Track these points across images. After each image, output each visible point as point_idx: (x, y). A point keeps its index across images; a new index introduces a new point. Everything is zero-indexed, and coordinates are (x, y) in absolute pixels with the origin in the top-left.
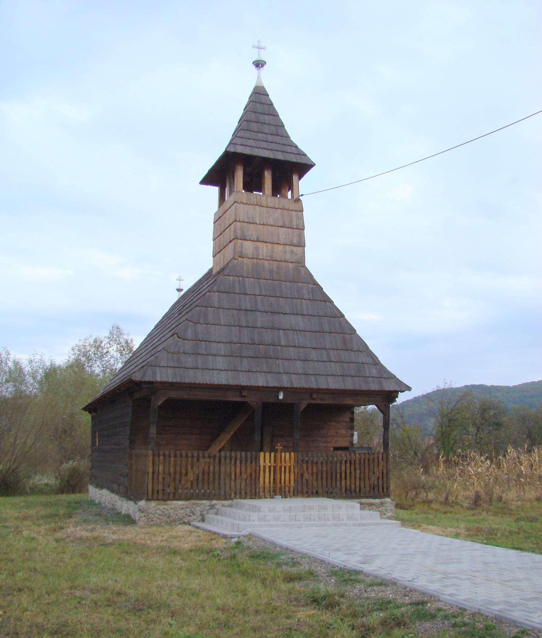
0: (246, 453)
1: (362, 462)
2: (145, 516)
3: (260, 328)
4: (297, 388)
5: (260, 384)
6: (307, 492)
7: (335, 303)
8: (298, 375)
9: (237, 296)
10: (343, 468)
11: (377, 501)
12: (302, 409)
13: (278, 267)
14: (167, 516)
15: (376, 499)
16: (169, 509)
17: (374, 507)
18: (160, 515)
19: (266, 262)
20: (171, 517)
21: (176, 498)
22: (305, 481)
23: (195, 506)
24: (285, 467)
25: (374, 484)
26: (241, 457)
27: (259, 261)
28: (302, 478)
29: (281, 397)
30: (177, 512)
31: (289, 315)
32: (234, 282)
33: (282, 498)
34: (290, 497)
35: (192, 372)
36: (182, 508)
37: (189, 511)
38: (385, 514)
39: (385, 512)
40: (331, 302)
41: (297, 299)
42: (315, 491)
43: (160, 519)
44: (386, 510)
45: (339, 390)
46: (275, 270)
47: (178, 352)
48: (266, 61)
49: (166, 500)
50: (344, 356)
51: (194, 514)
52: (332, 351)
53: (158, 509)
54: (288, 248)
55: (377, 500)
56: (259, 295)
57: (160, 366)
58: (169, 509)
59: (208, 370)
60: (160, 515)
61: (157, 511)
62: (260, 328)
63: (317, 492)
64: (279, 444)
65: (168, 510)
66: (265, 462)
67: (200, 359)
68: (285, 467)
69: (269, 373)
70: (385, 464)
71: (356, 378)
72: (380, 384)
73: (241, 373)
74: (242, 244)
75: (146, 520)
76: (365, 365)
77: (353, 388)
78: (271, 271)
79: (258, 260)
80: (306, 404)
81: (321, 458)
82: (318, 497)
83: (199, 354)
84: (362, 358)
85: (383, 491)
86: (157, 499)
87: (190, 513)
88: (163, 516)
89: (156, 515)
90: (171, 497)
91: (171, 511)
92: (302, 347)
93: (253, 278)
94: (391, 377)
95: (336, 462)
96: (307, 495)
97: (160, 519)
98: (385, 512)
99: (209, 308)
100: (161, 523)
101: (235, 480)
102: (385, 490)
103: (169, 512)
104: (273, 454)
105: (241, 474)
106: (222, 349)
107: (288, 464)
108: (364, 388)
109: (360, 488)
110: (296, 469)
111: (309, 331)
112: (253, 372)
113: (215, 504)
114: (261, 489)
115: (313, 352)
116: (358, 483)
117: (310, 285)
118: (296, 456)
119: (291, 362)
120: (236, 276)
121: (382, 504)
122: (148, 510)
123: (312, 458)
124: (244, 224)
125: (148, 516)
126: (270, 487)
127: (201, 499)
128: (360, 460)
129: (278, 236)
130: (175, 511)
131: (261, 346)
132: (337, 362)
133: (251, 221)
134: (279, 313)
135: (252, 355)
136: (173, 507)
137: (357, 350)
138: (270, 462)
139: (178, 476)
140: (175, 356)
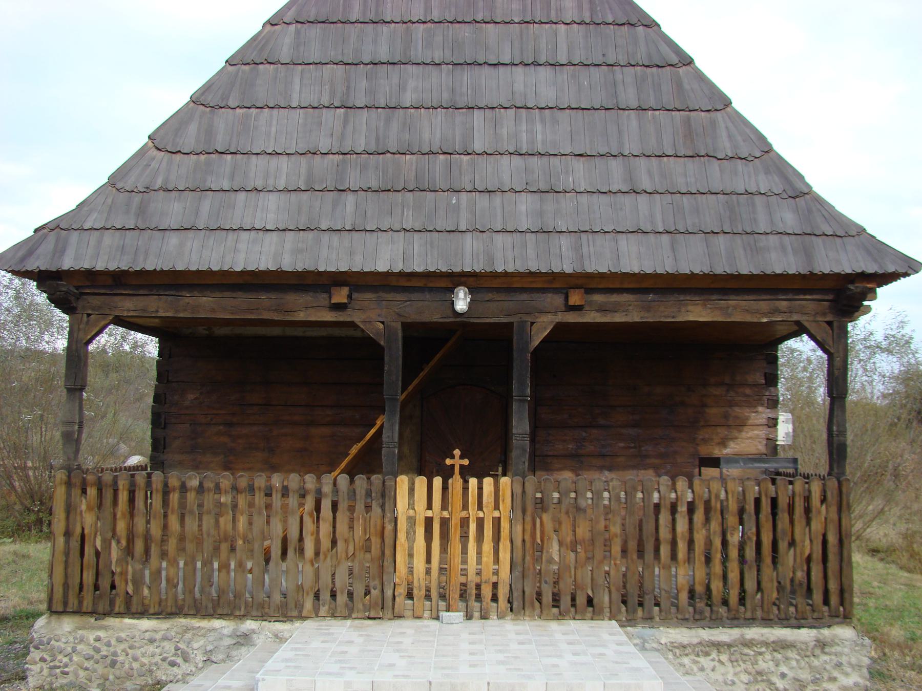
0: (369, 478)
2: (43, 660)
4: (506, 274)
9: (353, 30)
10: (682, 525)
11: (806, 635)
12: (536, 342)
14: (108, 660)
15: (799, 627)
17: (791, 654)
20: (118, 665)
23: (188, 636)
24: (480, 523)
25: (792, 580)
29: (462, 302)
30: (138, 653)
33: (469, 617)
34: (501, 617)
35: (173, 240)
36: (152, 641)
38: (833, 679)
39: (835, 674)
40: (651, 24)
43: (87, 669)
44: (839, 665)
45: (656, 276)
51: (186, 660)
53: (82, 641)
55: (804, 631)
58: (113, 642)
63: (590, 602)
64: (457, 452)
65: (108, 644)
66: (411, 505)
67: (207, 203)
68: (480, 523)
70: (834, 515)
71: (721, 237)
72: (808, 254)
73: (326, 237)
76: (758, 200)
77: (706, 270)
81: (606, 494)
83: (210, 190)
85: (826, 602)
86: (78, 612)
87: (175, 655)
89: (75, 658)
90: (119, 605)
95: (657, 507)
96: (555, 610)
98: (835, 674)
99: (261, 66)
102: (834, 599)
103: (112, 649)
104: (438, 481)
107: (489, 514)
108: (745, 267)
109: (743, 590)
110: (519, 528)
113: (253, 631)
114: (401, 591)
115: (579, 165)
116: (734, 576)
118: (518, 489)
119: (498, 199)
121: (822, 645)
122: (53, 642)
130: (131, 647)
131: (408, 157)
136: (123, 635)
138: (430, 506)
139: (139, 546)
140: (137, 198)
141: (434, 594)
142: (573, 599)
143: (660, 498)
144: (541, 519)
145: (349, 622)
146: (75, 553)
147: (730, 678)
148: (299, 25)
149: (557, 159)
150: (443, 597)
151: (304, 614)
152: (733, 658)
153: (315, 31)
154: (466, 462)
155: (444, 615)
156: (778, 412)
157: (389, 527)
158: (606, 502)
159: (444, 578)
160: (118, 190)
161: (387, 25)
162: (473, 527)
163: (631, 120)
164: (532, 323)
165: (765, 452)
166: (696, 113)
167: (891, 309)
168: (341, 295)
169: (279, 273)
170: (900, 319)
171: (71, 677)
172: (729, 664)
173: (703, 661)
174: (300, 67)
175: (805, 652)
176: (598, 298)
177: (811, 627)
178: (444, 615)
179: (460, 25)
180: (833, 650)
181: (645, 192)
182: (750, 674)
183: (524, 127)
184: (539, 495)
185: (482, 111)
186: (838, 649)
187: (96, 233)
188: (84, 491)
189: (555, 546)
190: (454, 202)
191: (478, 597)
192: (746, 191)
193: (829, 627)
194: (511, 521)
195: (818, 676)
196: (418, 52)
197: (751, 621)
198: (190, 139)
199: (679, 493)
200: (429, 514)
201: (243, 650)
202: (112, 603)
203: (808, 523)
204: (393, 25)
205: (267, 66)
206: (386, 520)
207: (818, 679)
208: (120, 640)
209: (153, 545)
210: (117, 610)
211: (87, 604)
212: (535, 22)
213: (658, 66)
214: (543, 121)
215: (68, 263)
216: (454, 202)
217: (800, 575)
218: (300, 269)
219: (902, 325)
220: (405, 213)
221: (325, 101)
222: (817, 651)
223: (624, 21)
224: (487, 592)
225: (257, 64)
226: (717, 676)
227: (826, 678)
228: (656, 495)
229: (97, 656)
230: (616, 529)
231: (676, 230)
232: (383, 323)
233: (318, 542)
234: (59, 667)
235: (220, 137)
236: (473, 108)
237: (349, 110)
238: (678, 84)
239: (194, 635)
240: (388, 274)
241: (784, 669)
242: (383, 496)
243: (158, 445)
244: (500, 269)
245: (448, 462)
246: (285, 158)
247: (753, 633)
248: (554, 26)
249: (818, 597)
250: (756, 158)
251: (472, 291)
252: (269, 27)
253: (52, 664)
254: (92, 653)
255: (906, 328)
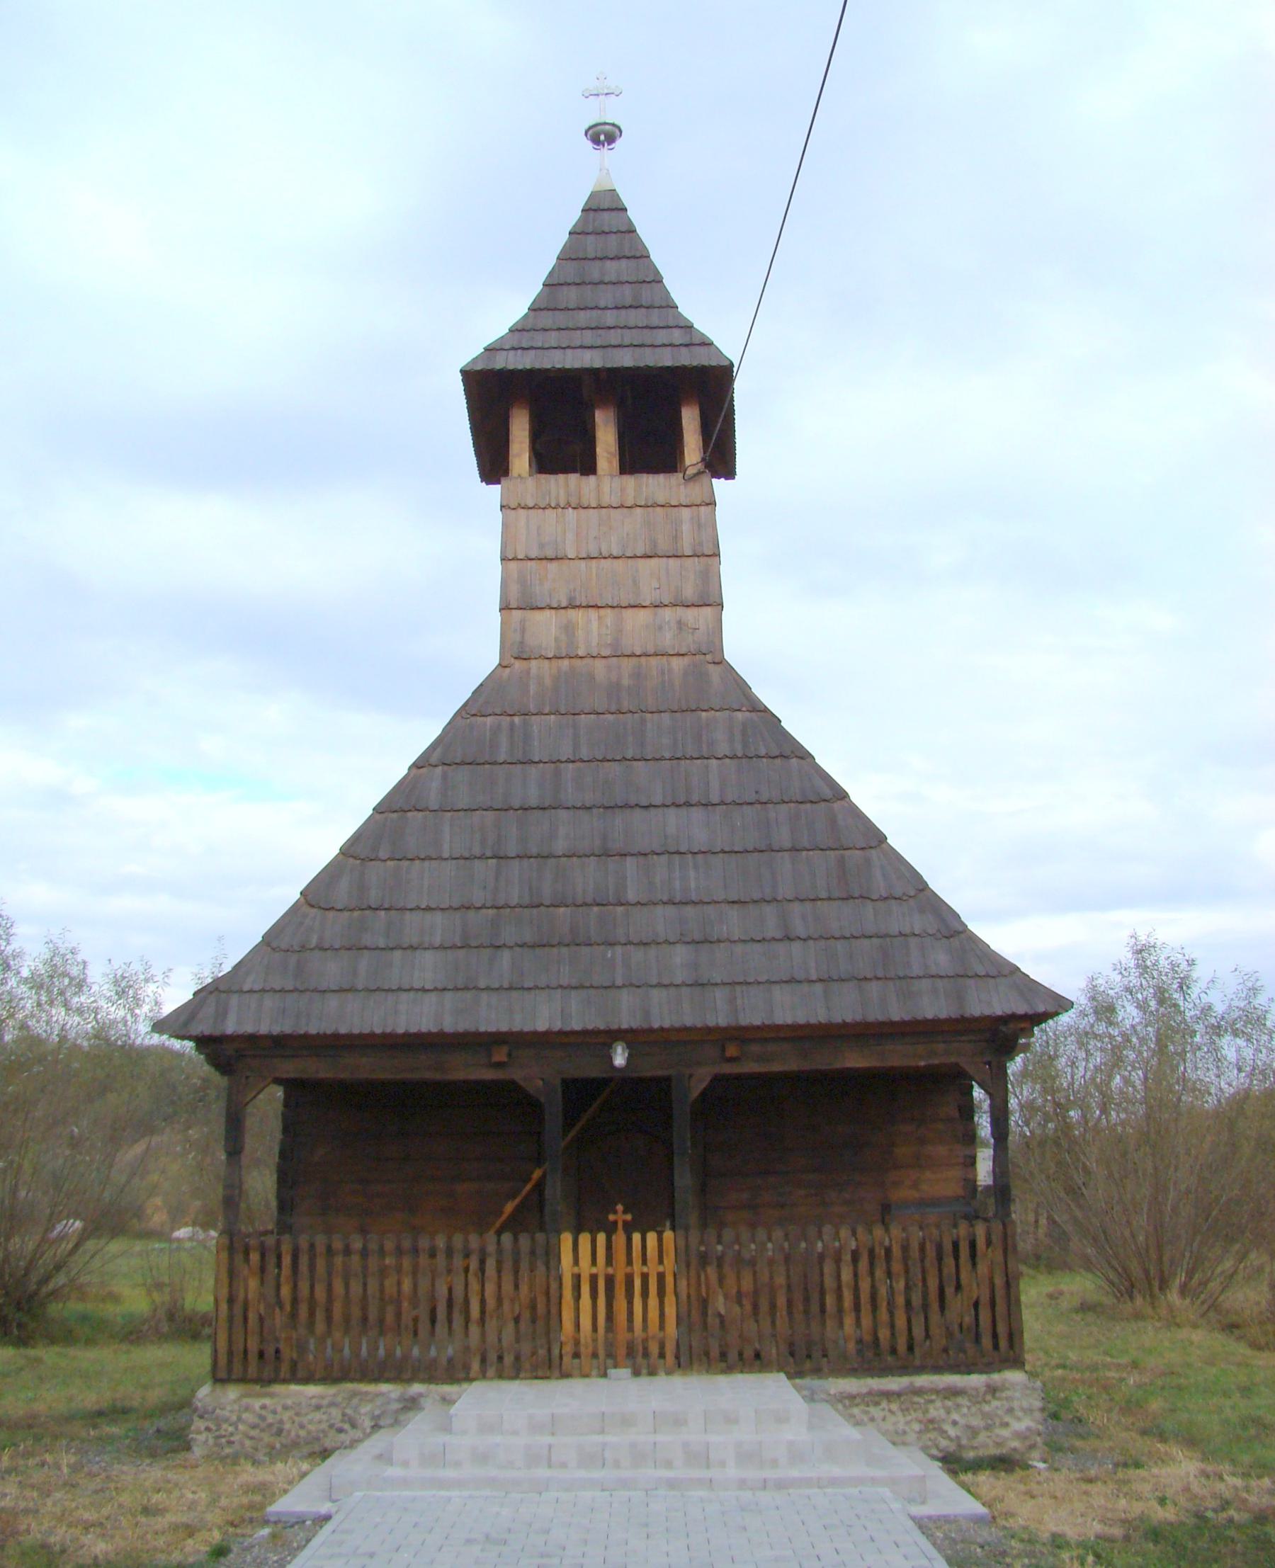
1: (915, 1253)
2: (208, 1429)
3: (565, 856)
4: (662, 1029)
5: (542, 1026)
6: (723, 1355)
7: (821, 761)
8: (672, 990)
9: (500, 771)
10: (846, 1275)
11: (976, 1380)
12: (695, 1094)
13: (638, 675)
14: (274, 1430)
15: (969, 1373)
16: (279, 1409)
17: (963, 1401)
18: (254, 1427)
19: (599, 664)
20: (284, 1434)
21: (300, 1374)
22: (713, 1321)
23: (355, 1401)
24: (645, 1277)
25: (961, 1326)
26: (500, 1251)
27: (577, 662)
28: (704, 1314)
29: (620, 1059)
30: (305, 1420)
31: (660, 810)
32: (496, 730)
34: (669, 1373)
35: (333, 1002)
36: (318, 1407)
37: (340, 1417)
38: (1007, 1425)
39: (1007, 1419)
41: (692, 758)
42: (749, 1353)
43: (252, 1438)
44: (1010, 1411)
46: (626, 682)
47: (303, 947)
48: (622, 128)
49: (271, 1381)
50: (839, 917)
51: (354, 1426)
52: (796, 908)
53: (247, 1409)
54: (667, 614)
56: (569, 761)
57: (241, 991)
58: (279, 1409)
59: (383, 994)
60: (254, 1427)
61: (245, 1416)
62: (565, 856)
63: (758, 1356)
64: (620, 1207)
65: (274, 1412)
66: (576, 1262)
67: (365, 962)
68: (645, 1277)
69: (576, 988)
70: (999, 1257)
73: (484, 996)
74: (523, 622)
75: (211, 1441)
76: (913, 942)
77: (858, 1018)
78: (614, 689)
79: (573, 661)
80: (709, 1079)
82: (760, 1371)
83: (366, 948)
84: (902, 919)
85: (996, 1346)
86: (243, 1380)
87: (343, 1421)
88: (262, 1430)
89: (241, 1427)
90: (285, 1370)
91: (286, 1416)
92: (694, 903)
93: (557, 713)
94: (1005, 972)
95: (822, 1257)
96: (723, 1365)
97: (252, 1438)
99: (409, 814)
100: (256, 1449)
101: (482, 1321)
102: (1003, 1343)
103: (278, 1417)
104: (601, 1237)
105: (499, 1300)
106: (439, 927)
108: (897, 1012)
110: (683, 1284)
111: (723, 852)
112: (523, 988)
113: (421, 1395)
114: (568, 1349)
115: (733, 913)
116: (901, 1322)
117: (739, 715)
118: (681, 1243)
119: (652, 951)
120: (504, 714)
121: (993, 1390)
122: (218, 1411)
123: (737, 1247)
124: (530, 563)
125: (219, 1427)
126: (595, 1340)
127: (377, 1380)
128: (905, 1248)
129: (635, 583)
130: (297, 1414)
131: (562, 910)
132: (810, 938)
133: (550, 554)
134: (627, 806)
135: (528, 937)
136: (289, 1402)
137: (884, 895)
139: (303, 1310)
140: (293, 959)
141: (601, 1352)
142: (741, 1354)
143: (824, 1246)
144: (705, 1271)
145: (517, 1382)
146: (238, 1318)
147: (901, 1428)
148: (446, 767)
149: (711, 907)
150: (610, 1355)
151: (472, 1375)
152: (903, 1407)
153: (462, 775)
154: (629, 1217)
155: (612, 1372)
156: (975, 1149)
157: (554, 1286)
158: (770, 1253)
159: (610, 1335)
160: (273, 949)
161: (535, 765)
162: (638, 1283)
163: (784, 862)
164: (691, 1076)
165: (963, 1194)
166: (849, 851)
167: (1236, 970)
168: (500, 1055)
169: (441, 1034)
170: (1250, 984)
171: (237, 1447)
172: (899, 1414)
173: (873, 1410)
174: (449, 814)
175: (977, 1398)
176: (755, 1048)
177: (981, 1372)
178: (612, 1372)
179: (610, 763)
180: (1004, 1395)
181: (799, 938)
182: (920, 1422)
183: (677, 874)
184: (703, 1248)
185: (634, 858)
186: (1009, 1393)
187: (256, 996)
188: (247, 1259)
189: (721, 1299)
190: (609, 955)
191: (646, 1354)
192: (900, 932)
193: (999, 1371)
194: (675, 1275)
195: (990, 1422)
196: (570, 795)
197: (921, 1370)
198: (342, 892)
199: (842, 1242)
200: (594, 1270)
201: (411, 1414)
202: (277, 1370)
203: (974, 1264)
204: (541, 765)
205: (416, 813)
206: (551, 1279)
207: (990, 1425)
208: (285, 1408)
209: (318, 1309)
210: (282, 1375)
211: (252, 1370)
212: (686, 758)
213: (812, 802)
214: (696, 867)
215: (230, 1027)
216: (609, 955)
217: (968, 1320)
218: (461, 1030)
219: (1254, 991)
220: (562, 970)
221: (477, 851)
222: (989, 1397)
223: (777, 754)
224: (654, 1349)
225: (405, 811)
226: (888, 1425)
227: (997, 1424)
228: (820, 1245)
229: (263, 1425)
230: (780, 1280)
231: (829, 977)
232: (542, 1079)
233: (483, 1302)
234: (224, 1436)
235: (373, 893)
236: (625, 855)
237: (501, 860)
238: (833, 821)
239: (361, 1400)
240: (547, 1033)
241: (955, 1416)
242: (547, 1254)
243: (285, 1206)
244: (656, 1025)
245: (612, 1217)
246: (439, 913)
247: (922, 1380)
248: (705, 761)
249: (987, 1341)
250: (910, 897)
251: (630, 1046)
252: (414, 771)
253: (217, 1433)
254: (256, 1420)
255: (1259, 996)
